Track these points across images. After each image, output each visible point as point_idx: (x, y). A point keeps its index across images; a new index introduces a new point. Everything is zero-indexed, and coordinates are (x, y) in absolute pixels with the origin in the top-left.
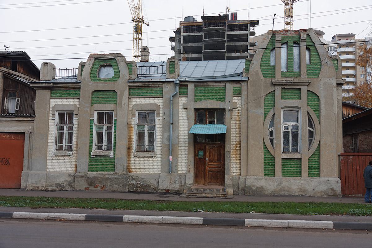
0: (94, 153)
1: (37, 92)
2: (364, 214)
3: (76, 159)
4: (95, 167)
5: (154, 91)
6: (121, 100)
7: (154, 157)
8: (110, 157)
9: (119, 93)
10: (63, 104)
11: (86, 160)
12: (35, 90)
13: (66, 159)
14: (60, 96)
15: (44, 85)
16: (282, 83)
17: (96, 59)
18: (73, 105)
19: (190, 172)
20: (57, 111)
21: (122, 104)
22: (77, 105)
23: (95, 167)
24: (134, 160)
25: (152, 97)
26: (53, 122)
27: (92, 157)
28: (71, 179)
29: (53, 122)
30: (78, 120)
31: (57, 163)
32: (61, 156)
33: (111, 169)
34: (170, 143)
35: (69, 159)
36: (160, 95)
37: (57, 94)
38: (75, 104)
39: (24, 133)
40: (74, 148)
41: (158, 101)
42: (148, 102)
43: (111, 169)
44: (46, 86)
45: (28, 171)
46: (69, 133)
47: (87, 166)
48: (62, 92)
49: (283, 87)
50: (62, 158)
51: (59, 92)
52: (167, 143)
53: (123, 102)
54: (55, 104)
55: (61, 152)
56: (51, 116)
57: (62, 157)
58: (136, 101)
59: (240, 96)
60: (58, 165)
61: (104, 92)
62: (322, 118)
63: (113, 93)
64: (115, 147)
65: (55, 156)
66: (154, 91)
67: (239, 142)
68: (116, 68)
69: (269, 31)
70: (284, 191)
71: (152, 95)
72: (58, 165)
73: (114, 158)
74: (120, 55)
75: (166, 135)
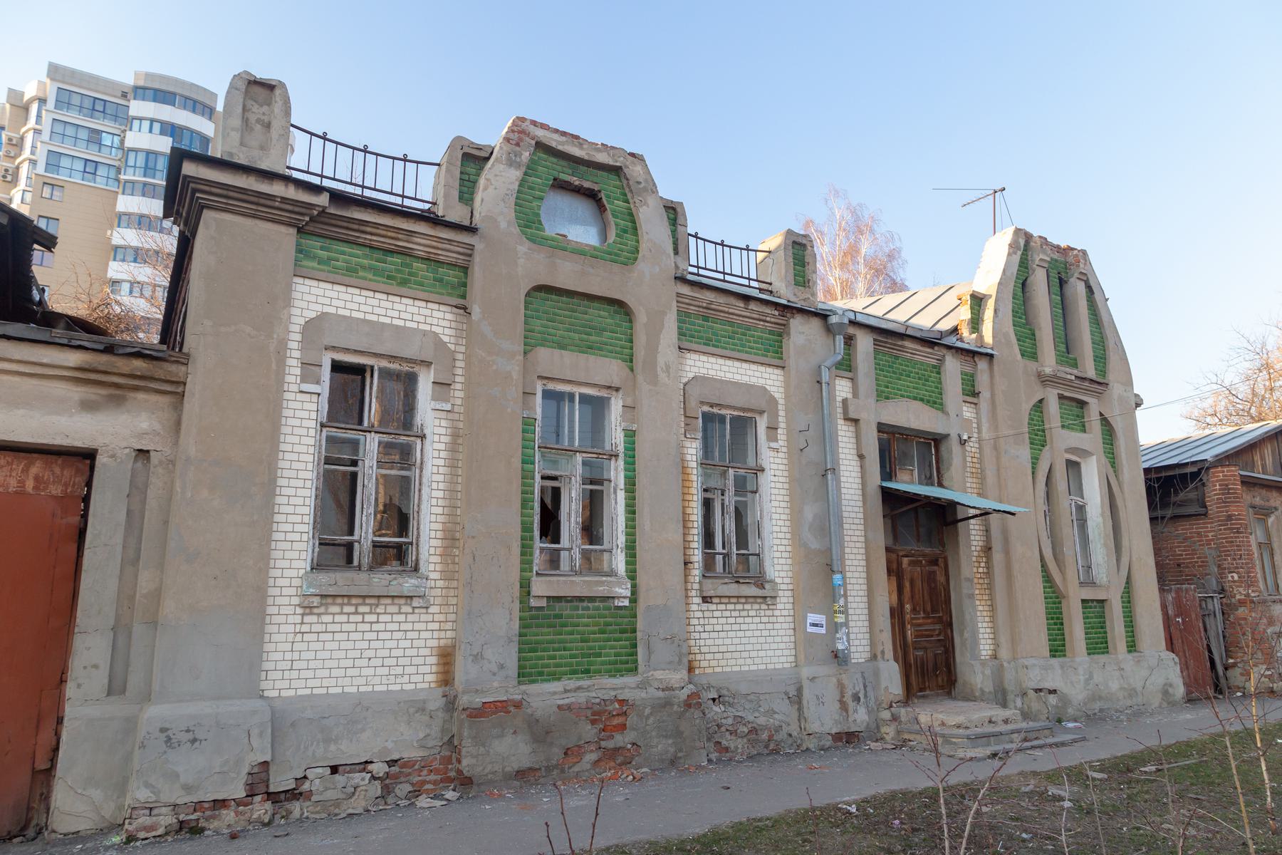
0: (540, 587)
1: (205, 211)
2: (902, 746)
3: (442, 618)
4: (551, 658)
5: (753, 336)
6: (653, 349)
7: (767, 600)
8: (617, 603)
9: (641, 318)
10: (369, 317)
11: (505, 620)
12: (202, 207)
13: (388, 618)
14: (348, 276)
15: (277, 189)
16: (1064, 379)
17: (540, 146)
18: (425, 333)
19: (886, 657)
20: (541, 377)
21: (659, 369)
22: (446, 339)
23: (551, 658)
24: (700, 614)
25: (745, 356)
26: (307, 406)
27: (533, 603)
28: (428, 731)
29: (307, 406)
30: (450, 416)
31: (328, 646)
32: (339, 600)
33: (622, 663)
34: (831, 544)
35: (402, 618)
36: (774, 352)
37: (330, 259)
38: (434, 329)
39: (148, 451)
40: (433, 559)
41: (768, 379)
42: (745, 379)
43: (622, 663)
44: (284, 200)
45: (117, 708)
46: (588, 494)
47: (514, 649)
48: (358, 256)
49: (1060, 392)
50: (363, 614)
51: (347, 255)
52: (815, 545)
53: (661, 361)
54: (319, 308)
55: (340, 580)
56: (298, 371)
57: (361, 609)
58: (701, 365)
59: (975, 400)
60: (337, 654)
61: (596, 305)
62: (1126, 487)
63: (615, 312)
64: (634, 556)
65: (316, 601)
66: (753, 336)
67: (986, 547)
68: (621, 213)
69: (245, 72)
70: (1100, 698)
71: (747, 352)
72: (337, 654)
73: (632, 612)
74: (282, 85)
75: (810, 513)
